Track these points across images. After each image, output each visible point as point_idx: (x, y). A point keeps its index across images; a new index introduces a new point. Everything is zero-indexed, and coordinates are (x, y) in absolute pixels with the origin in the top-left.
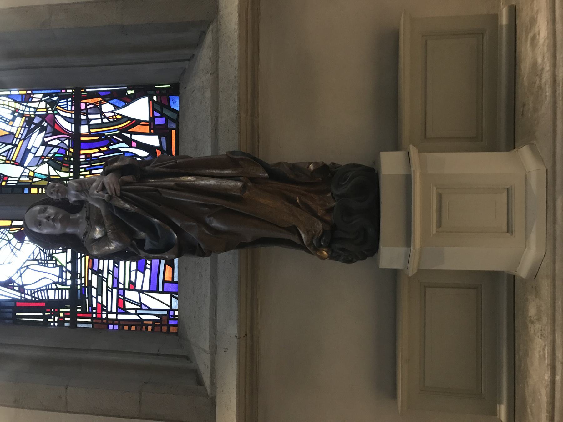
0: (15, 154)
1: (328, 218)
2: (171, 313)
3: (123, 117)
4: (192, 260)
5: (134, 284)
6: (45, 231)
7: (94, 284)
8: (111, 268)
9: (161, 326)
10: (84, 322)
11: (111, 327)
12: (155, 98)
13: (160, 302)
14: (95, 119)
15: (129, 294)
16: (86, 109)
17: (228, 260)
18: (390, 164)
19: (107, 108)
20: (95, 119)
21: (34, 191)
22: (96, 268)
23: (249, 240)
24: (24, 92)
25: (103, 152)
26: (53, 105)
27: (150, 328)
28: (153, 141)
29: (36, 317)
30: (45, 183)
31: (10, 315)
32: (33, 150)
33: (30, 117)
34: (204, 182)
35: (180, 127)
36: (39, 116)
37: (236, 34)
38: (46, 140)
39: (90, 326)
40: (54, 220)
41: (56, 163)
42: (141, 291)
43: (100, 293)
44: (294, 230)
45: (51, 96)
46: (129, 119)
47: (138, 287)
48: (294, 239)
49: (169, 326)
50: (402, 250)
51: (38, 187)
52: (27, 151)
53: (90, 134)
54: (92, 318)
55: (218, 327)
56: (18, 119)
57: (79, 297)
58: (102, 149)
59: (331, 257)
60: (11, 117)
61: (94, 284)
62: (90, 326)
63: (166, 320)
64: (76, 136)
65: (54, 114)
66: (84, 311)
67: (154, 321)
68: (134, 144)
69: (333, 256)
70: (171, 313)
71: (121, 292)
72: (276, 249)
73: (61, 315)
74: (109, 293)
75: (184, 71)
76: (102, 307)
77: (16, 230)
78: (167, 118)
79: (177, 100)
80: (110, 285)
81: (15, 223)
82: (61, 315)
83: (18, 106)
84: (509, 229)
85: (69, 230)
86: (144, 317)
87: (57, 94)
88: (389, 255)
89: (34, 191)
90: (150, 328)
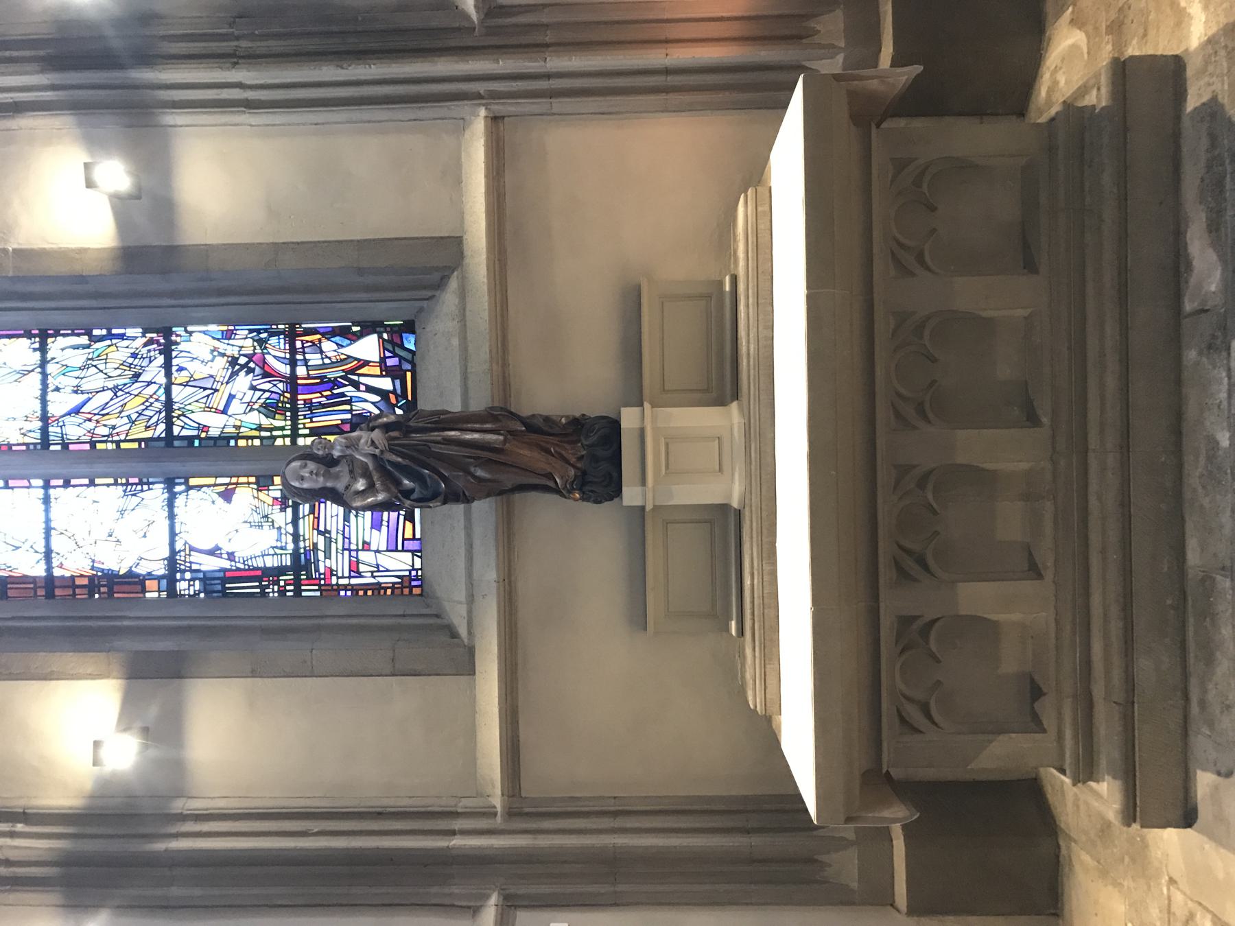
0: (219, 401)
1: (579, 465)
2: (414, 573)
3: (349, 357)
4: (441, 511)
5: (369, 544)
6: (306, 485)
7: (321, 546)
8: (341, 528)
9: (402, 588)
10: (310, 591)
11: (342, 593)
12: (385, 336)
13: (400, 563)
14: (315, 359)
15: (363, 556)
16: (303, 347)
17: (483, 508)
18: (629, 419)
19: (328, 346)
20: (315, 359)
21: (242, 443)
22: (322, 528)
23: (509, 486)
24: (225, 328)
25: (326, 397)
26: (262, 342)
27: (389, 592)
28: (386, 384)
29: (251, 587)
30: (256, 433)
31: (219, 587)
32: (239, 396)
33: (233, 357)
34: (468, 436)
35: (418, 369)
36: (245, 356)
37: (485, 288)
38: (255, 383)
39: (318, 594)
40: (317, 475)
41: (270, 409)
42: (378, 551)
43: (328, 556)
44: (550, 476)
45: (259, 332)
46: (356, 359)
47: (374, 547)
48: (551, 484)
49: (411, 588)
50: (639, 489)
51: (247, 438)
52: (231, 397)
53: (309, 377)
54: (319, 585)
55: (475, 576)
56: (219, 359)
57: (302, 564)
58: (325, 393)
59: (583, 499)
60: (210, 357)
61: (321, 546)
62: (318, 594)
63: (406, 583)
64: (292, 380)
65: (263, 354)
66: (309, 578)
67: (394, 584)
68: (363, 388)
69: (584, 498)
70: (414, 573)
71: (354, 554)
72: (533, 495)
73: (282, 583)
74: (340, 556)
75: (421, 310)
76: (331, 572)
77: (222, 489)
78: (401, 358)
79: (412, 338)
80: (340, 547)
81: (220, 480)
82: (282, 583)
83: (217, 344)
84: (721, 470)
85: (329, 484)
86: (382, 580)
87: (266, 330)
88: (631, 495)
89: (242, 443)
90: (389, 592)
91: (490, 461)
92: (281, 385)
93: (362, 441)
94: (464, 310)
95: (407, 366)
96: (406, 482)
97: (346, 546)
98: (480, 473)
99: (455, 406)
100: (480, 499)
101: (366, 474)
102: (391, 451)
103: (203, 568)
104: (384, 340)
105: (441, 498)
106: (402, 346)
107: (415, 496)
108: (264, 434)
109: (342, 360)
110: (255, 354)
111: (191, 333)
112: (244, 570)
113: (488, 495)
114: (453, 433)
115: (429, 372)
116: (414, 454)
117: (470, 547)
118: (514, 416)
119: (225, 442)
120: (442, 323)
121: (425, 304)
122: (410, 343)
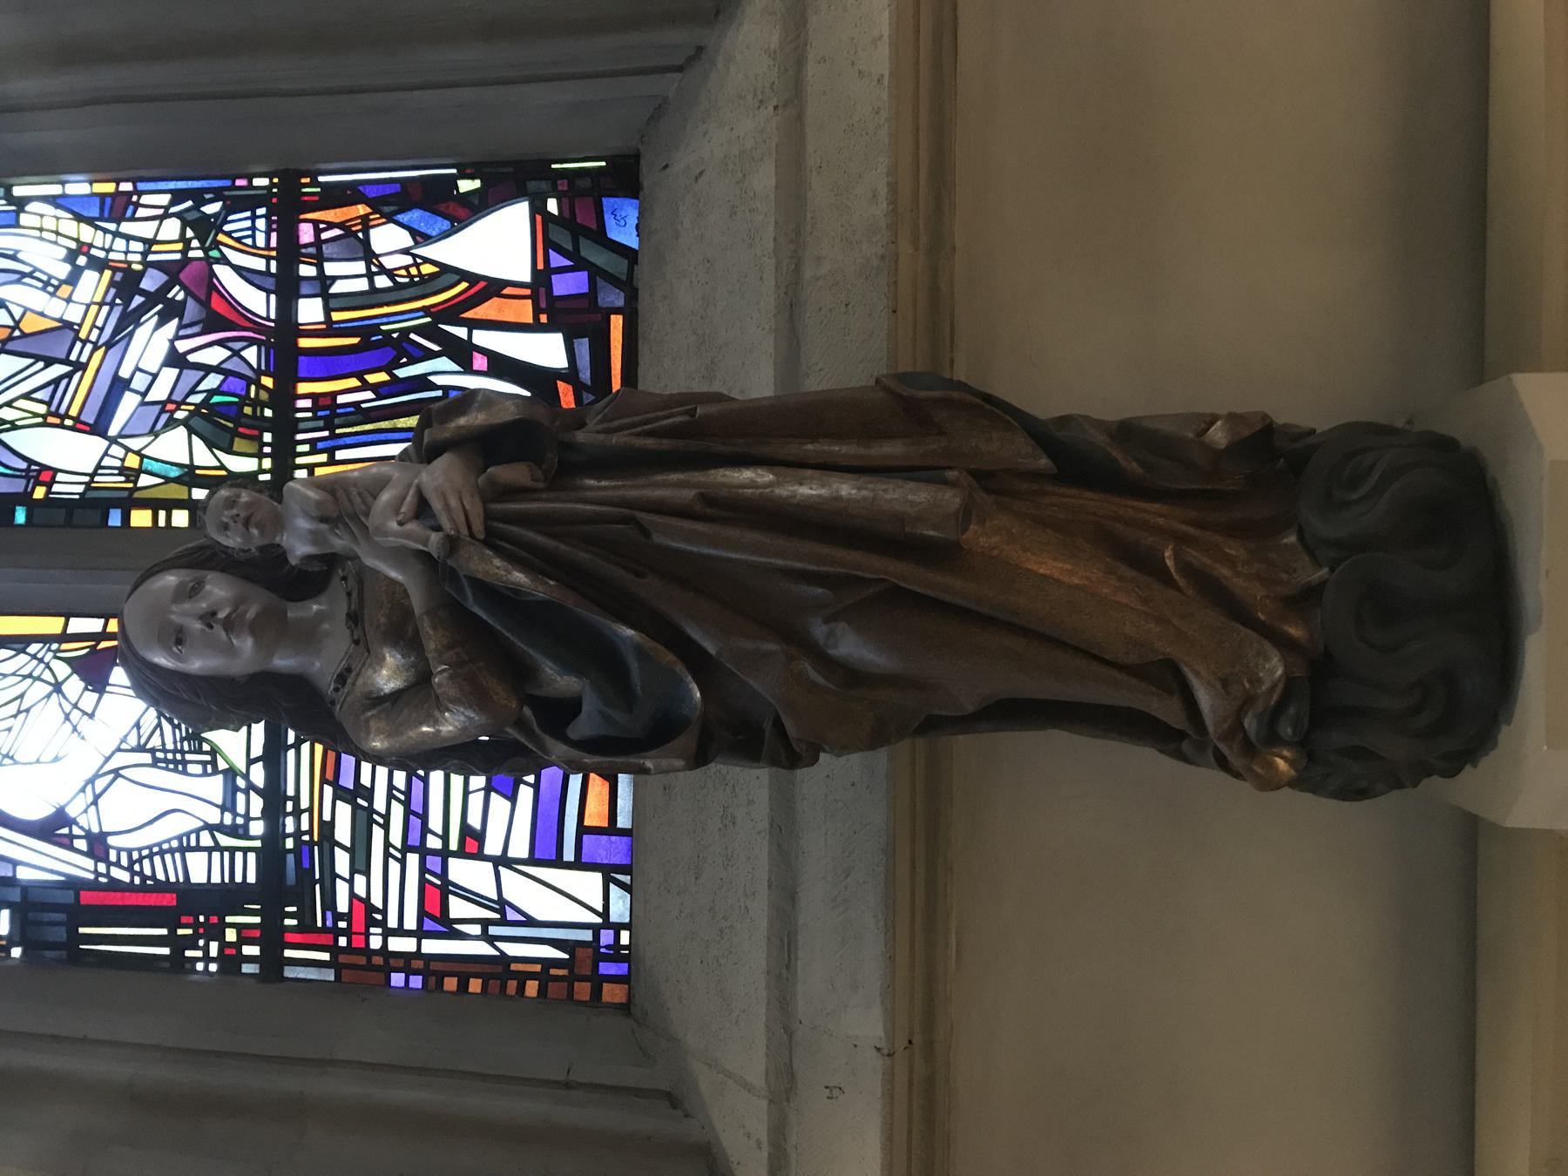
0: (80, 395)
2: (607, 937)
3: (445, 269)
5: (480, 837)
7: (343, 833)
9: (571, 980)
10: (307, 961)
11: (397, 979)
12: (552, 206)
13: (567, 899)
14: (348, 275)
15: (462, 872)
16: (318, 242)
19: (388, 239)
20: (348, 275)
21: (141, 518)
24: (109, 188)
26: (206, 228)
27: (532, 988)
28: (547, 351)
29: (144, 941)
31: (61, 934)
32: (139, 382)
33: (127, 270)
34: (807, 490)
35: (644, 303)
36: (158, 265)
38: (182, 346)
39: (329, 975)
40: (228, 625)
41: (215, 423)
42: (503, 861)
43: (361, 864)
45: (199, 197)
47: (493, 847)
48: (1169, 711)
49: (598, 981)
51: (154, 505)
52: (119, 386)
53: (330, 329)
54: (333, 949)
56: (90, 277)
57: (289, 878)
58: (372, 378)
61: (343, 833)
62: (329, 975)
63: (587, 960)
65: (209, 261)
66: (306, 925)
68: (480, 362)
70: (607, 937)
71: (434, 863)
73: (231, 935)
74: (394, 867)
75: (659, 109)
76: (368, 913)
77: (78, 650)
78: (595, 273)
80: (396, 838)
81: (78, 625)
82: (231, 935)
83: (86, 233)
85: (283, 662)
86: (512, 949)
87: (218, 195)
89: (141, 518)
90: (532, 988)
91: (897, 597)
92: (251, 354)
93: (386, 496)
94: (800, 63)
95: (613, 297)
96: (549, 669)
97: (414, 840)
98: (850, 646)
99: (757, 382)
100: (842, 749)
101: (403, 634)
102: (492, 540)
103: (23, 874)
104: (548, 216)
105: (687, 741)
106: (600, 236)
107: (582, 727)
108: (199, 494)
109: (426, 279)
110: (186, 261)
111: (21, 203)
112: (130, 887)
113: (876, 740)
114: (747, 474)
115: (674, 301)
116: (583, 556)
117: (786, 895)
118: (994, 411)
119: (94, 516)
120: (725, 143)
121: (670, 85)
122: (623, 229)
